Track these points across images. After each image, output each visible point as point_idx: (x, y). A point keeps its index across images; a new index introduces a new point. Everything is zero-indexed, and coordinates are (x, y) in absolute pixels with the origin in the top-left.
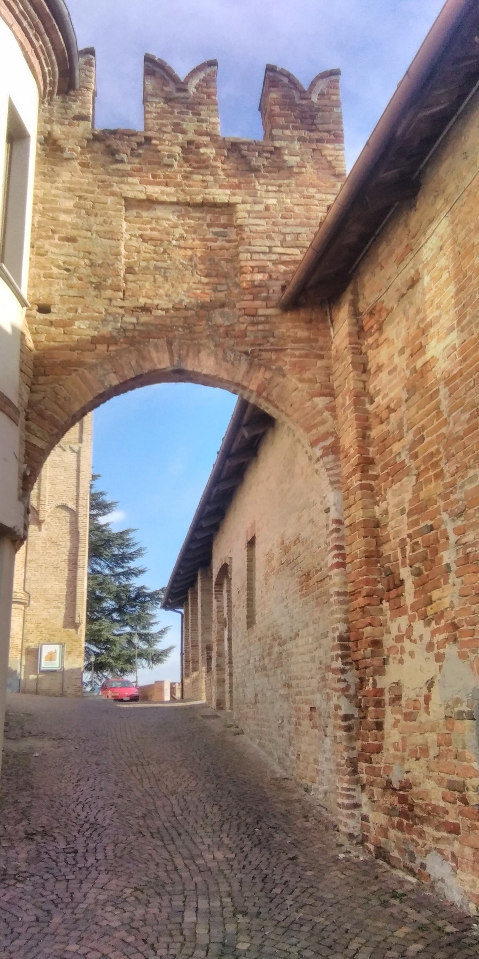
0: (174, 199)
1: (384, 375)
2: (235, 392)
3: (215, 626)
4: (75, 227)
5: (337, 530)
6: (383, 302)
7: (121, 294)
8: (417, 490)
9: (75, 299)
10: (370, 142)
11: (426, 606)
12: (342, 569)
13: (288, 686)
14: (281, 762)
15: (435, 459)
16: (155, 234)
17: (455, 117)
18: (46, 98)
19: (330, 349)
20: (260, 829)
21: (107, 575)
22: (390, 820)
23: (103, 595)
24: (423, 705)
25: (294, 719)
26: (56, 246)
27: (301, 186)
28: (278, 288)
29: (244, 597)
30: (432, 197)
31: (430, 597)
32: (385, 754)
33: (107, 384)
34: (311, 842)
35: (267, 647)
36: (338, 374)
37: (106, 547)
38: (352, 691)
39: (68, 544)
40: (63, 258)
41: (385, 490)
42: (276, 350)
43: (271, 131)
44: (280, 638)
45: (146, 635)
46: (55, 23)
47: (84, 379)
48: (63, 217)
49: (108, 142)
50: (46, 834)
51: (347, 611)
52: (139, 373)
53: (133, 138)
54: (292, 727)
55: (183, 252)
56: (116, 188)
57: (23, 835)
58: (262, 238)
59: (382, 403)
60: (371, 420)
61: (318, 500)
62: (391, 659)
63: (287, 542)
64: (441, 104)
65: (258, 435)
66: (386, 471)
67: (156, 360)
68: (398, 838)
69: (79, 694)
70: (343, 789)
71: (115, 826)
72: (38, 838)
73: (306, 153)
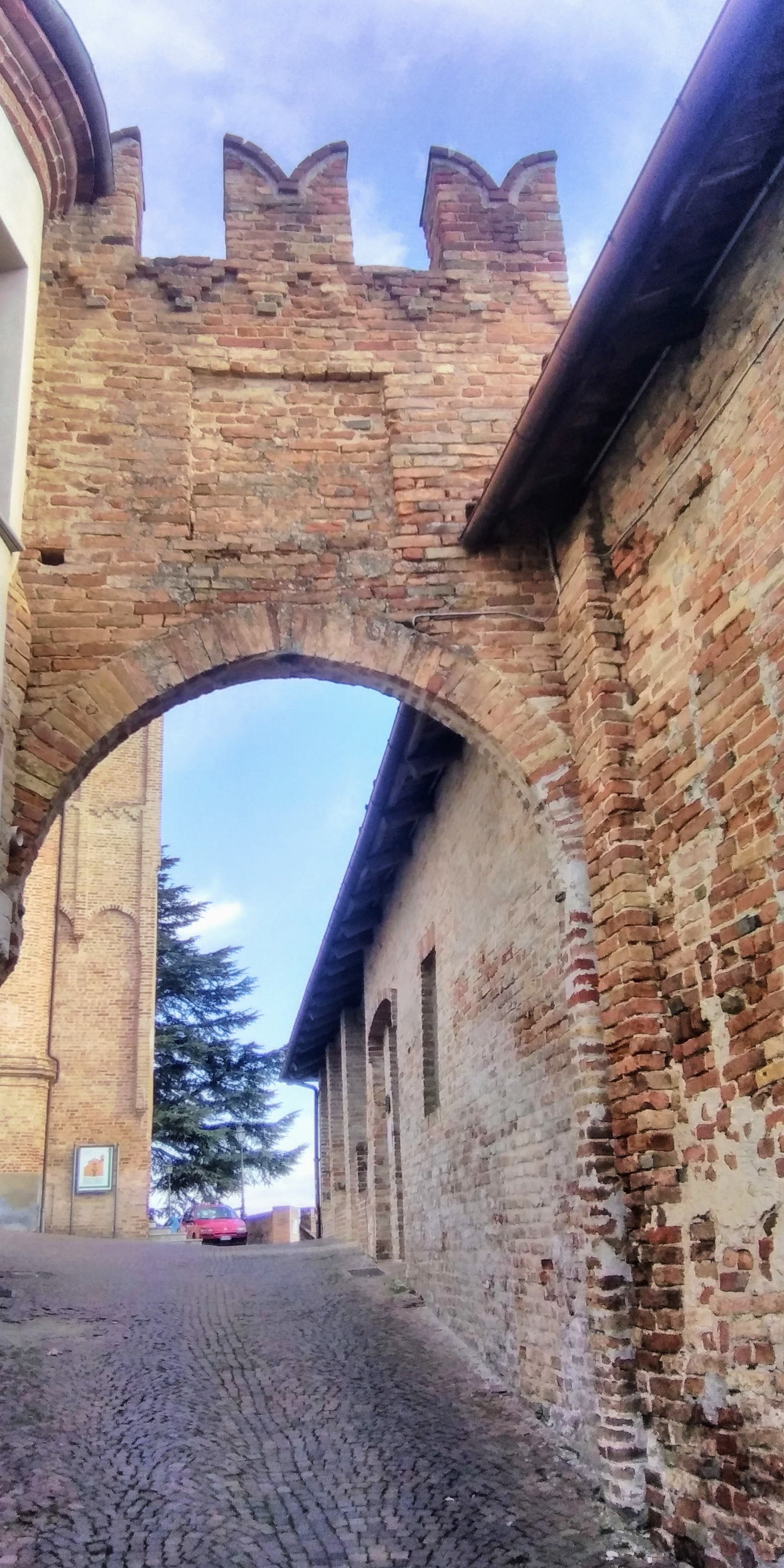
0: (278, 370)
1: (653, 652)
2: (389, 693)
3: (371, 1111)
4: (106, 418)
5: (581, 933)
6: (647, 524)
7: (185, 529)
8: (725, 855)
9: (106, 539)
10: (615, 236)
11: (754, 1069)
12: (592, 1003)
13: (501, 1220)
14: (491, 1358)
15: (757, 795)
17: (765, 190)
18: (57, 209)
19: (555, 614)
20: (455, 1496)
21: (193, 1026)
22: (703, 1485)
23: (187, 1059)
24: (758, 1261)
26: (74, 451)
27: (496, 342)
28: (461, 514)
29: (418, 1057)
30: (729, 334)
31: (762, 1053)
32: (688, 1356)
33: (162, 683)
34: (552, 1524)
35: (461, 1148)
36: (570, 654)
37: (182, 974)
38: (619, 1232)
39: (125, 975)
40: (85, 471)
41: (665, 857)
42: (460, 618)
43: (441, 256)
45: (258, 1127)
46: (66, 78)
47: (120, 674)
48: (85, 403)
49: (163, 279)
50: (56, 1513)
51: (604, 1081)
52: (220, 662)
53: (206, 271)
55: (293, 457)
56: (176, 353)
57: (15, 1515)
58: (431, 429)
59: (652, 700)
60: (633, 732)
61: (543, 880)
62: (690, 1171)
63: (490, 959)
64: (741, 165)
65: (436, 772)
66: (666, 822)
67: (248, 640)
68: (719, 1522)
69: (143, 1232)
70: (609, 1420)
71: (187, 1496)
72: (41, 1521)
73: (503, 288)
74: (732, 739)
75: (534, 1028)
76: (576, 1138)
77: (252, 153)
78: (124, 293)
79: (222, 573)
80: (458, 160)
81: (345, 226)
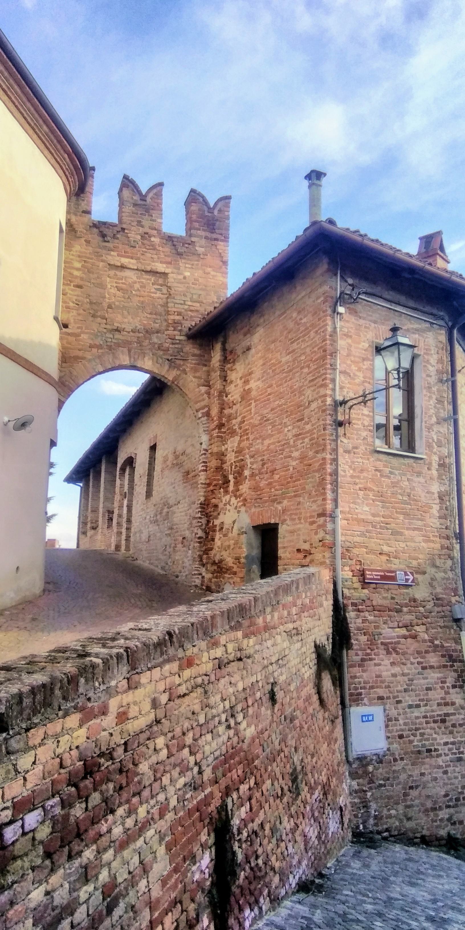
0: (136, 268)
1: (232, 386)
4: (82, 279)
5: (205, 454)
8: (239, 444)
13: (171, 529)
16: (124, 286)
25: (173, 545)
26: (72, 290)
29: (145, 479)
35: (159, 509)
40: (75, 297)
42: (183, 360)
44: (168, 504)
49: (101, 229)
51: (205, 492)
54: (172, 549)
55: (138, 298)
56: (104, 258)
74: (244, 417)
75: (188, 476)
76: (197, 505)
77: (132, 182)
78: (88, 233)
79: (116, 337)
80: (200, 194)
81: (160, 216)
